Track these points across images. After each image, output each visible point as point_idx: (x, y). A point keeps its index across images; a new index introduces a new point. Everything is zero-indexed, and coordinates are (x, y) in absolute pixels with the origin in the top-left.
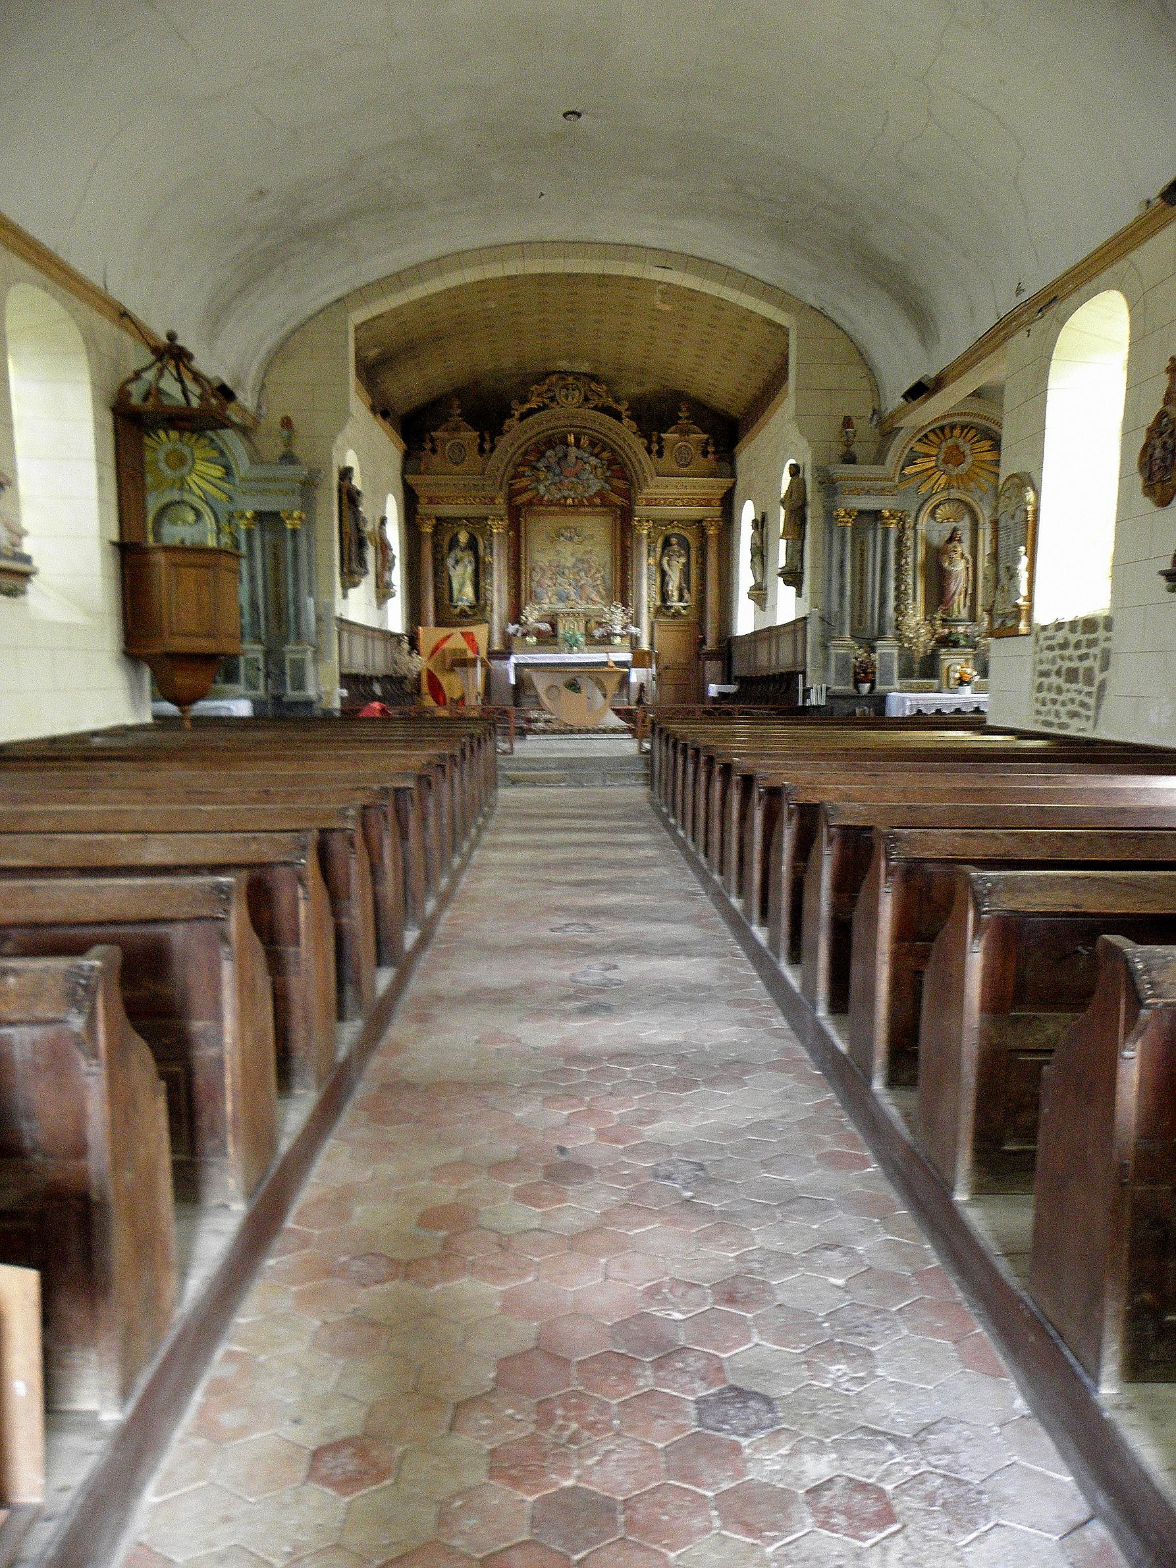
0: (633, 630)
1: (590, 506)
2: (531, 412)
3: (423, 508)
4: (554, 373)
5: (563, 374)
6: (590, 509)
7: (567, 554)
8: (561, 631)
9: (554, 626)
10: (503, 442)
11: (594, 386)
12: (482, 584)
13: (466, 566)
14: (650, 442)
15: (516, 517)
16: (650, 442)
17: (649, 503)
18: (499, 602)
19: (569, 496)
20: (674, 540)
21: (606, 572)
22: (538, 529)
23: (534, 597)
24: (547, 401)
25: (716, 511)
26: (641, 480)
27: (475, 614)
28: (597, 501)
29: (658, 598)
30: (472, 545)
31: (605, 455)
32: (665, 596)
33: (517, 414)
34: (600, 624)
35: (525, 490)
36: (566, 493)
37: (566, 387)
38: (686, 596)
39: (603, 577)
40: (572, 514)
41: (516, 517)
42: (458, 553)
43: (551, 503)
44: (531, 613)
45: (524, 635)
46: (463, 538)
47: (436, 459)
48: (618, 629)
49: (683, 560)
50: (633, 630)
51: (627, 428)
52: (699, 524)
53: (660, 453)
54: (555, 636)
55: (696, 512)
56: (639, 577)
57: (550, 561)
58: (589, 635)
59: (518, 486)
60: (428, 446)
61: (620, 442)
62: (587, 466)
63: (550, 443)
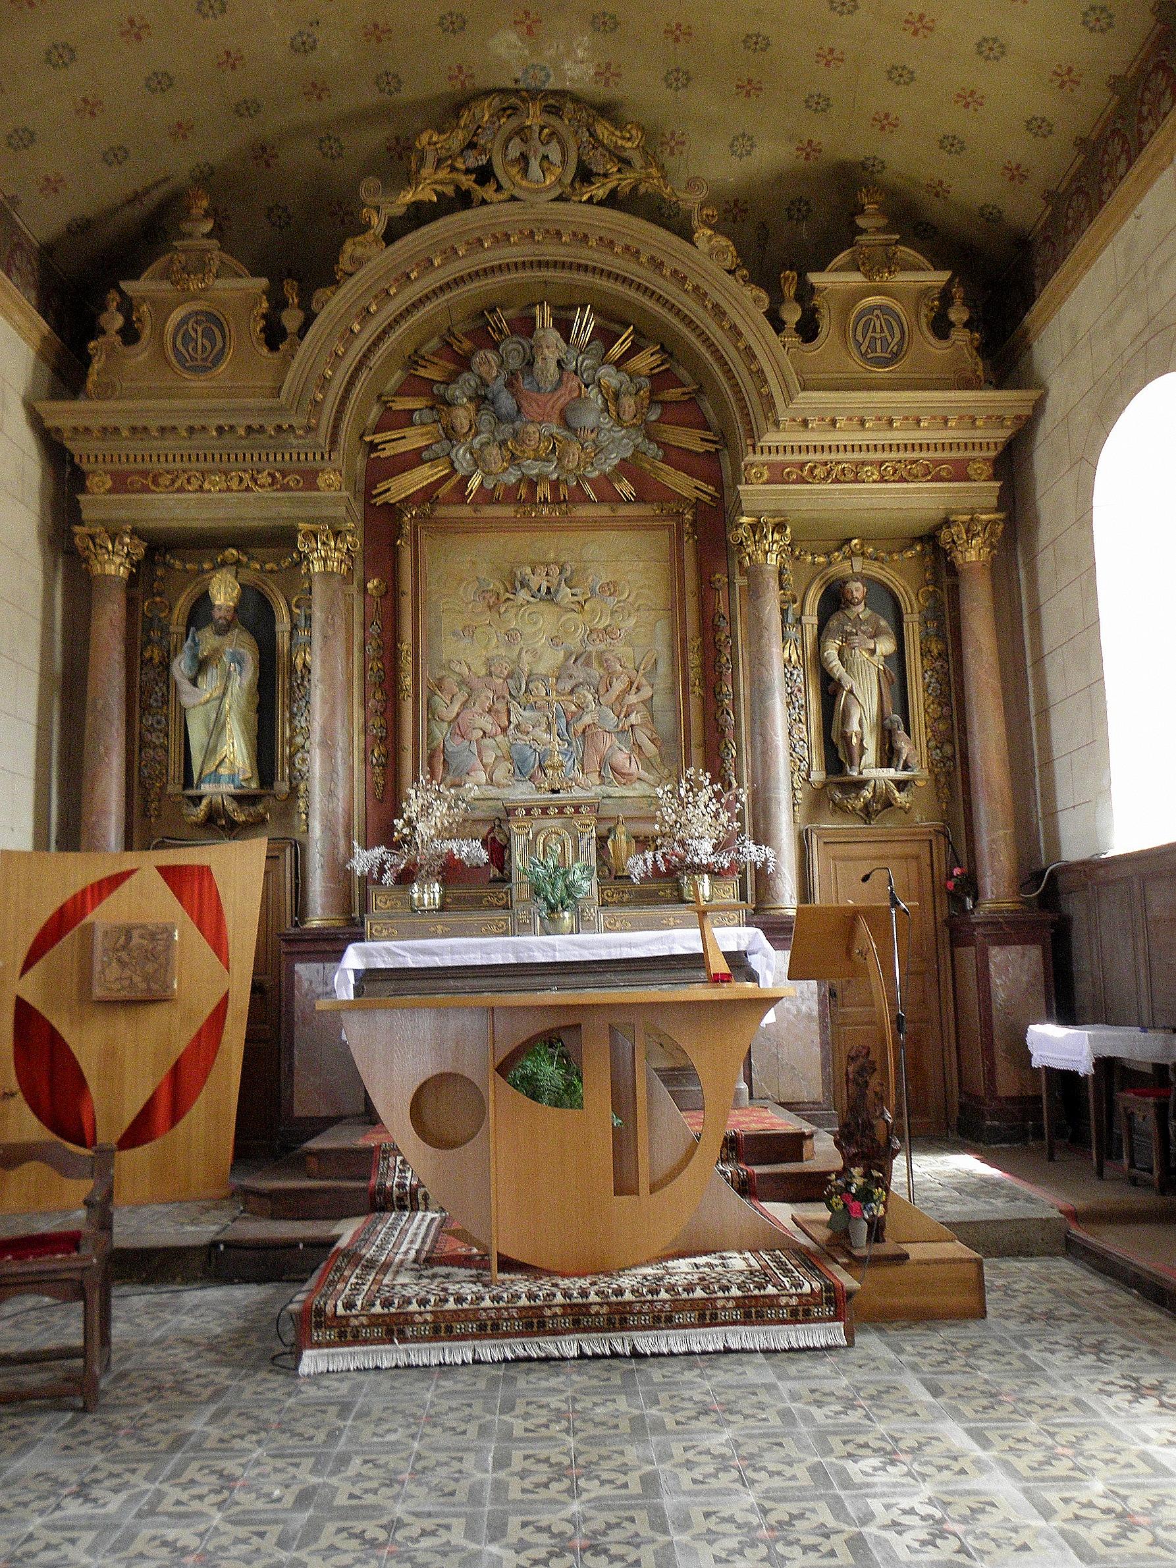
0: (752, 852)
1: (602, 500)
2: (420, 215)
3: (98, 502)
4: (488, 93)
5: (512, 99)
6: (604, 510)
7: (539, 639)
8: (519, 860)
9: (499, 852)
10: (334, 304)
11: (604, 131)
14: (777, 299)
15: (386, 539)
16: (777, 299)
17: (778, 475)
18: (330, 775)
19: (542, 477)
20: (857, 590)
21: (658, 687)
22: (453, 577)
23: (442, 766)
24: (467, 182)
25: (983, 492)
26: (753, 401)
28: (625, 488)
29: (817, 760)
30: (255, 615)
31: (645, 361)
32: (836, 752)
33: (378, 224)
34: (643, 843)
35: (415, 459)
36: (534, 469)
37: (522, 133)
38: (905, 746)
39: (648, 702)
40: (550, 525)
41: (386, 539)
42: (208, 640)
43: (487, 496)
44: (426, 810)
45: (406, 878)
46: (224, 593)
47: (141, 354)
48: (704, 851)
49: (886, 646)
50: (752, 852)
51: (709, 254)
52: (932, 544)
53: (808, 330)
54: (506, 879)
55: (921, 500)
56: (760, 694)
57: (488, 662)
58: (611, 875)
59: (389, 451)
60: (114, 321)
61: (690, 305)
62: (593, 392)
63: (484, 337)
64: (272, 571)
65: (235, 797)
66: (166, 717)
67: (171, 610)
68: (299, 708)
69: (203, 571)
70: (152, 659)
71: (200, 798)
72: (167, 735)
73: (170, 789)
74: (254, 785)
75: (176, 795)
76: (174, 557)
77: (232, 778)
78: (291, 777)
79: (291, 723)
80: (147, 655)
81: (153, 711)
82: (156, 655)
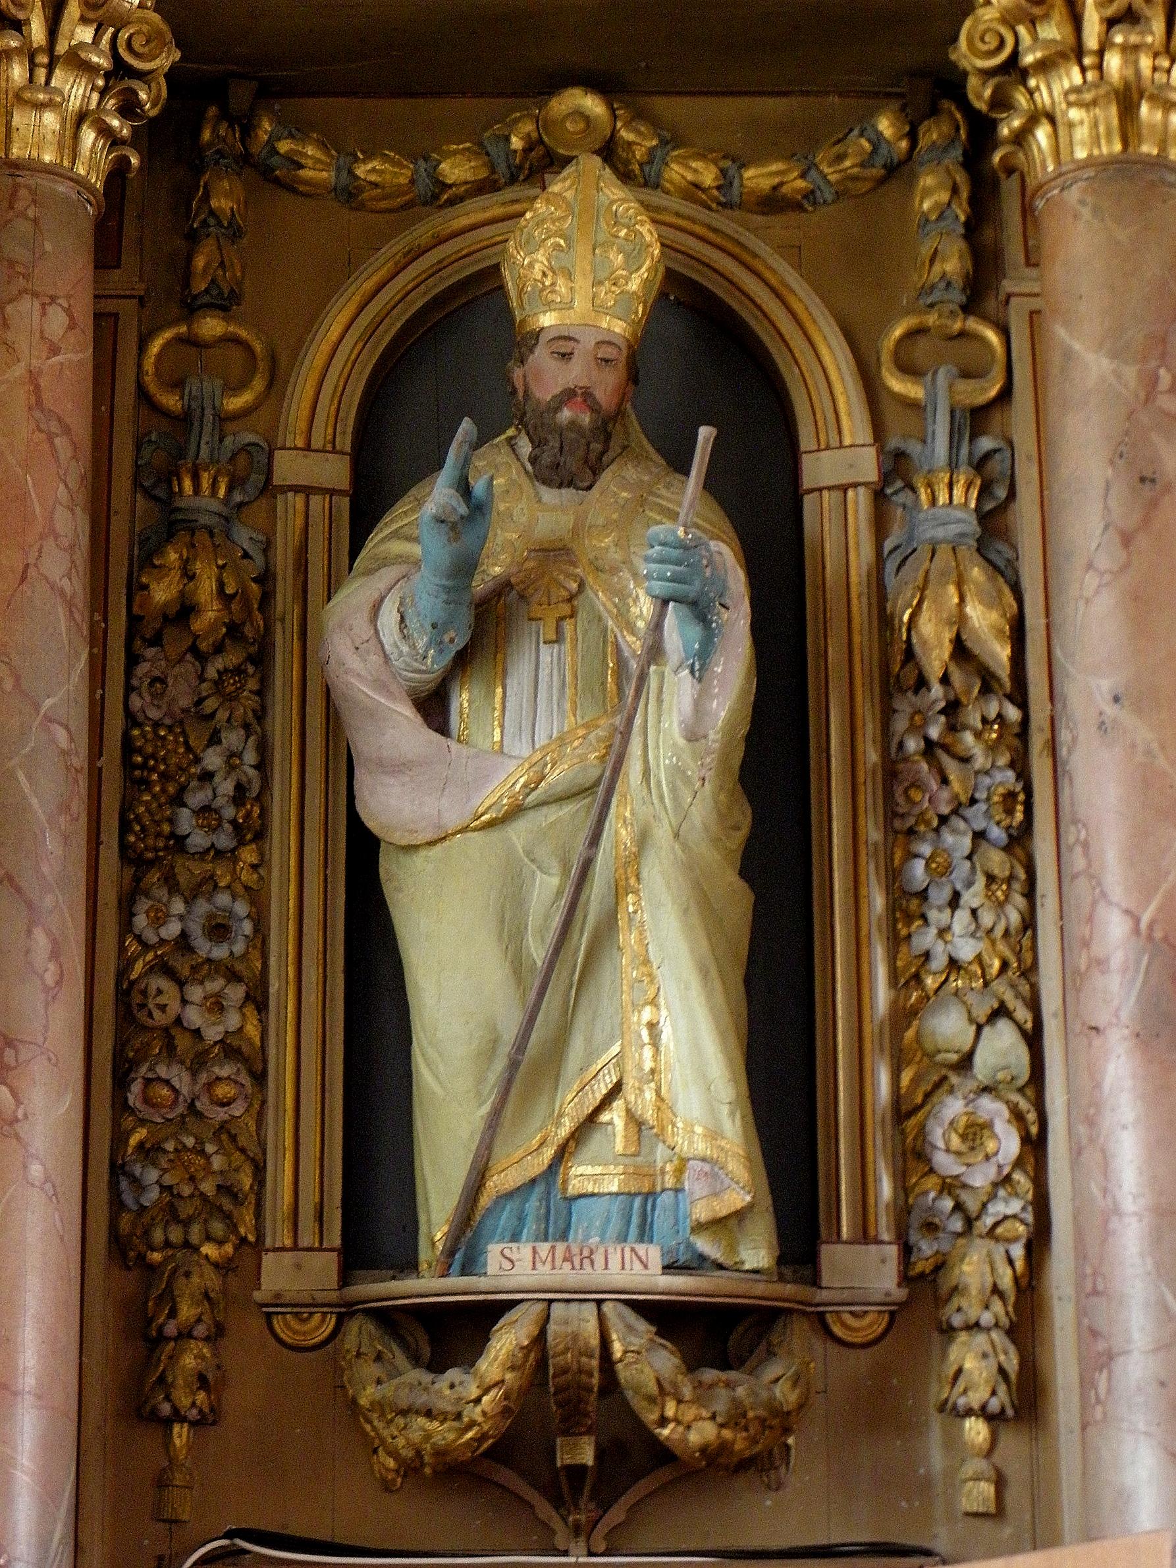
12: (861, 985)
13: (621, 688)
27: (747, 1463)
35: (214, 486)
46: (581, 272)
64: (773, 203)
65: (664, 1316)
66: (257, 898)
67: (277, 382)
68: (940, 869)
69: (438, 196)
70: (186, 610)
71: (485, 1315)
72: (258, 999)
73: (278, 1275)
74: (757, 1253)
75: (302, 1308)
76: (299, 129)
77: (640, 1210)
78: (908, 1221)
79: (896, 942)
80: (162, 592)
81: (188, 871)
82: (206, 589)
